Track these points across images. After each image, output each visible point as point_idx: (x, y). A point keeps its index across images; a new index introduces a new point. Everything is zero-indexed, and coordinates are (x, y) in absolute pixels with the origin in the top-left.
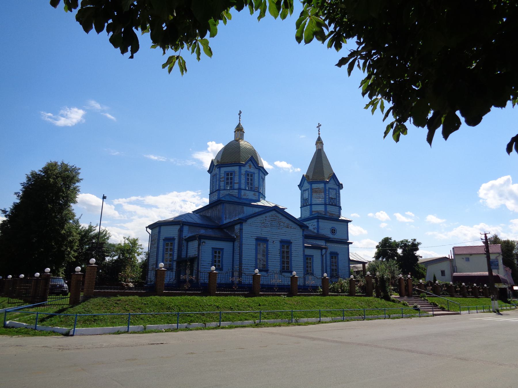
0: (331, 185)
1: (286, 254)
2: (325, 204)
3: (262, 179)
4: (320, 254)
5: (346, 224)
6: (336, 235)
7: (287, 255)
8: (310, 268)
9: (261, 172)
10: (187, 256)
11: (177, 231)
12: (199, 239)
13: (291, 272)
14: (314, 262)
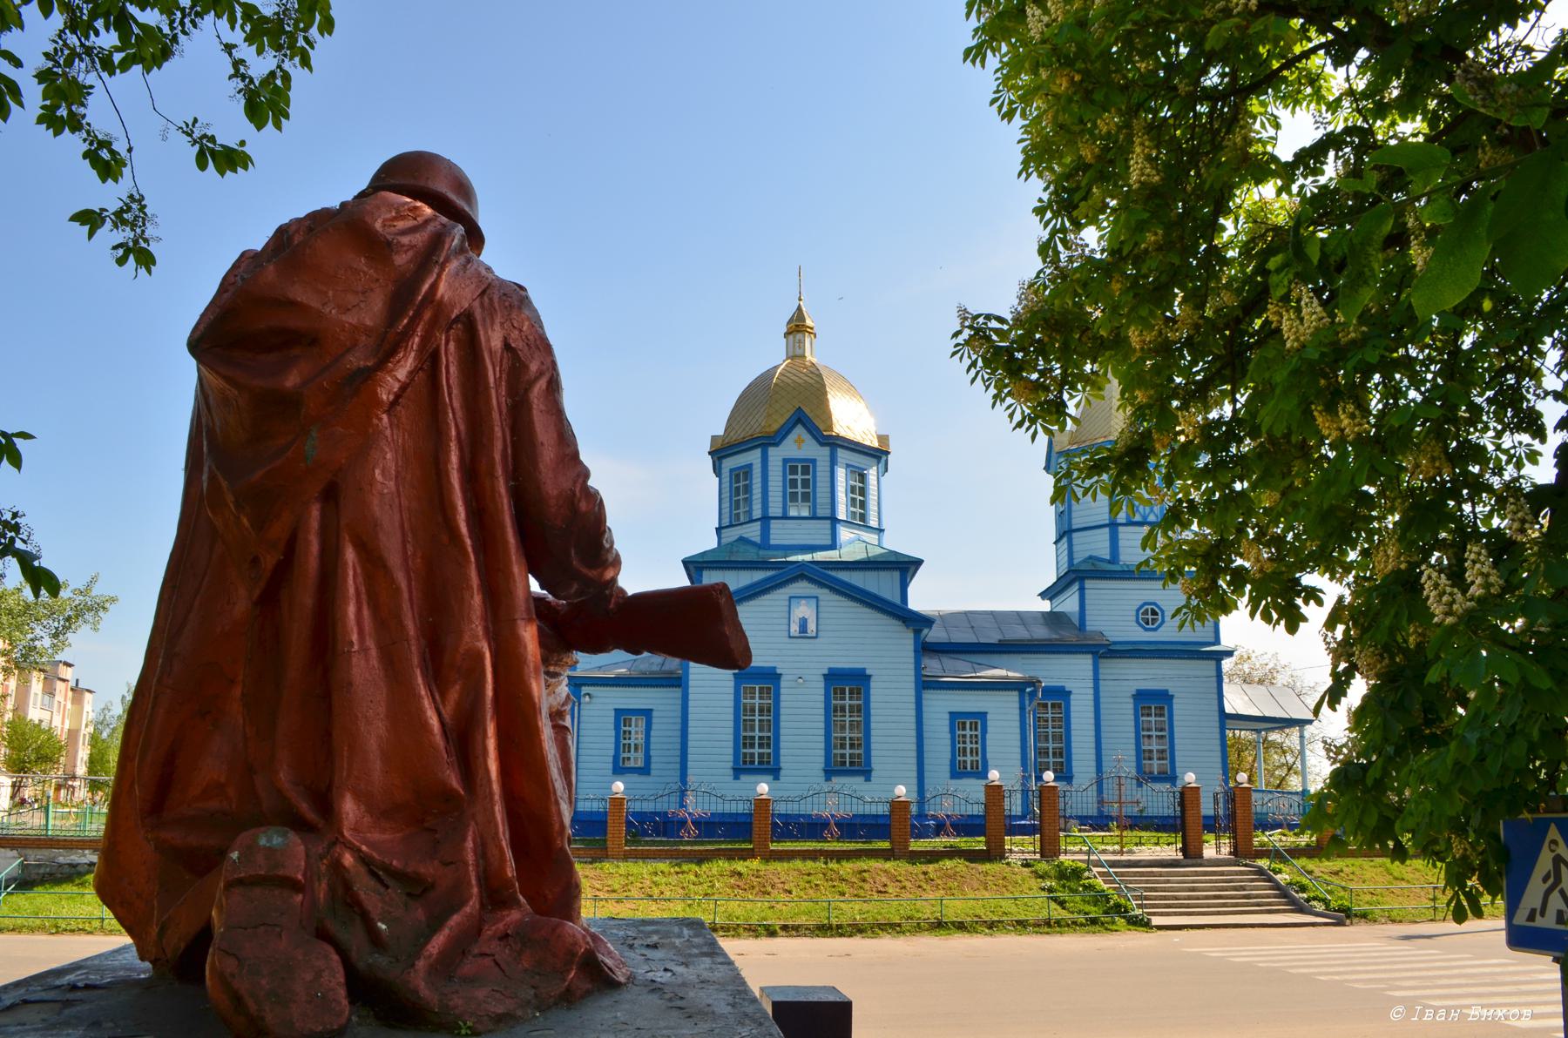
13: (983, 775)
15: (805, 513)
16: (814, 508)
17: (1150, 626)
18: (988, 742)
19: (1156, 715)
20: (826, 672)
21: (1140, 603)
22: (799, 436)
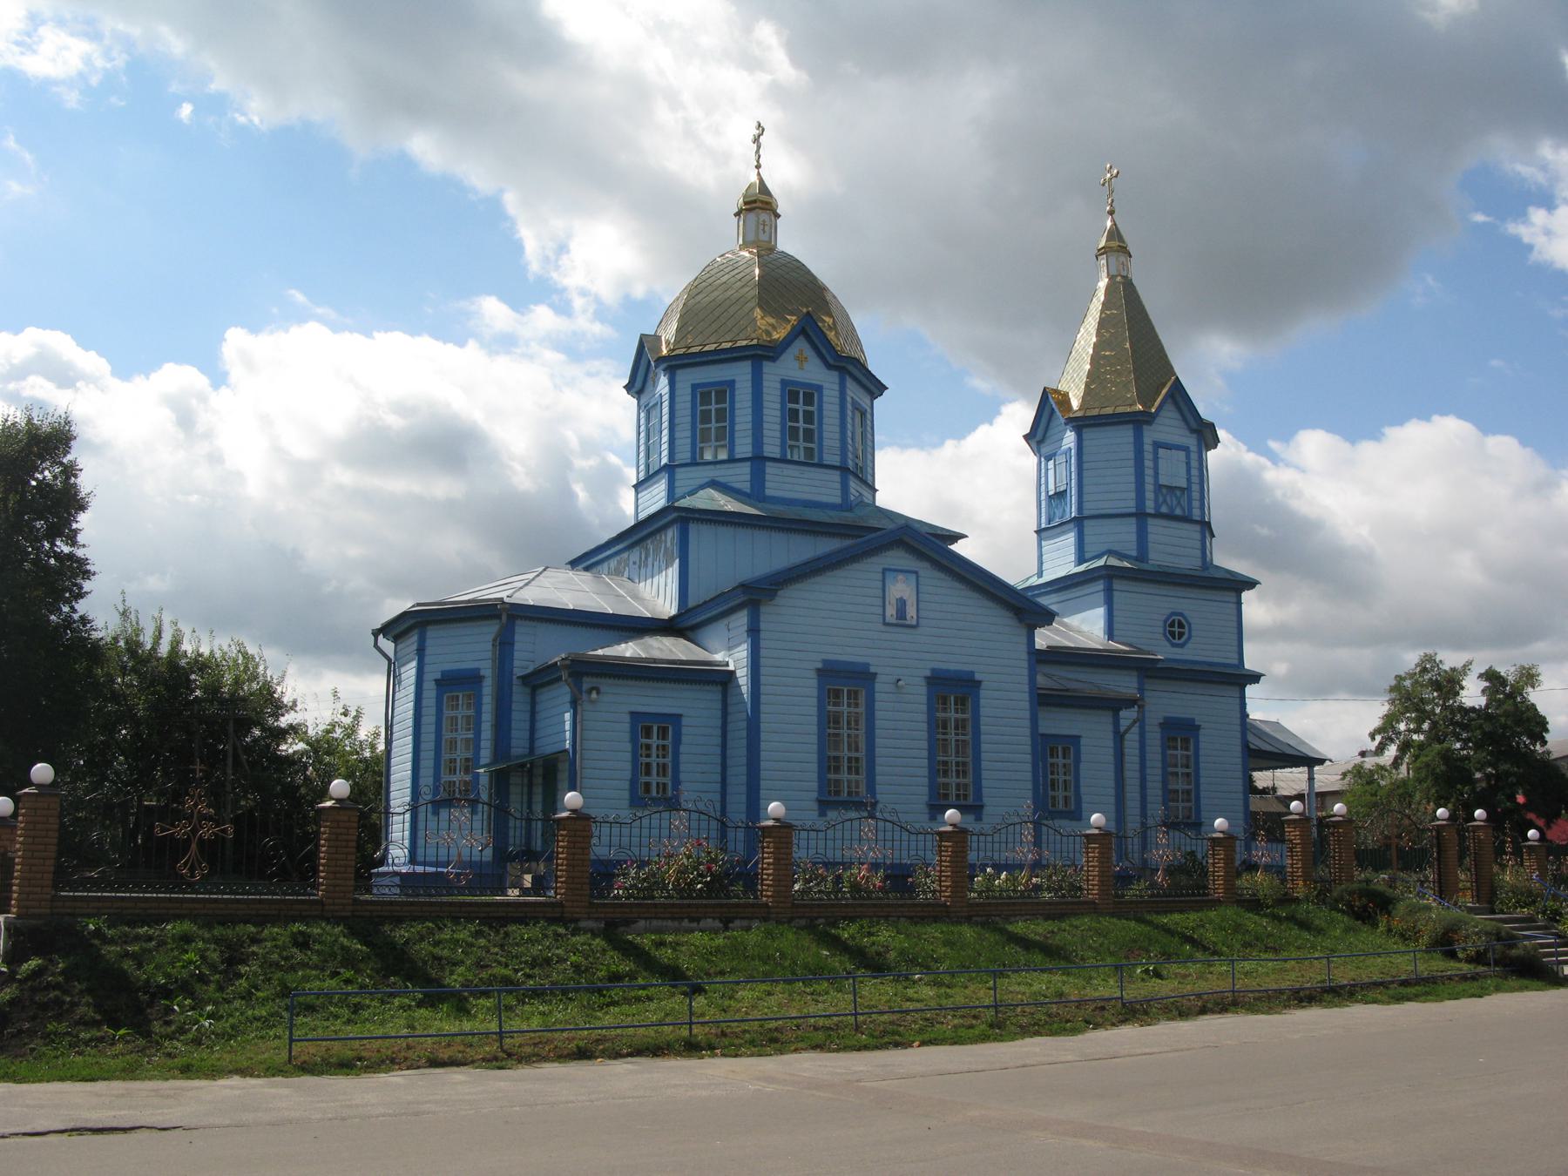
0: (1168, 428)
1: (957, 734)
2: (1141, 516)
3: (858, 415)
4: (1110, 728)
5: (1231, 596)
6: (1189, 645)
7: (961, 737)
8: (1066, 789)
9: (850, 384)
10: (532, 749)
11: (490, 647)
12: (570, 675)
14: (1083, 766)
15: (723, 456)
16: (731, 451)
17: (1176, 641)
18: (1083, 773)
19: (1182, 749)
20: (928, 673)
21: (1170, 611)
22: (801, 351)
